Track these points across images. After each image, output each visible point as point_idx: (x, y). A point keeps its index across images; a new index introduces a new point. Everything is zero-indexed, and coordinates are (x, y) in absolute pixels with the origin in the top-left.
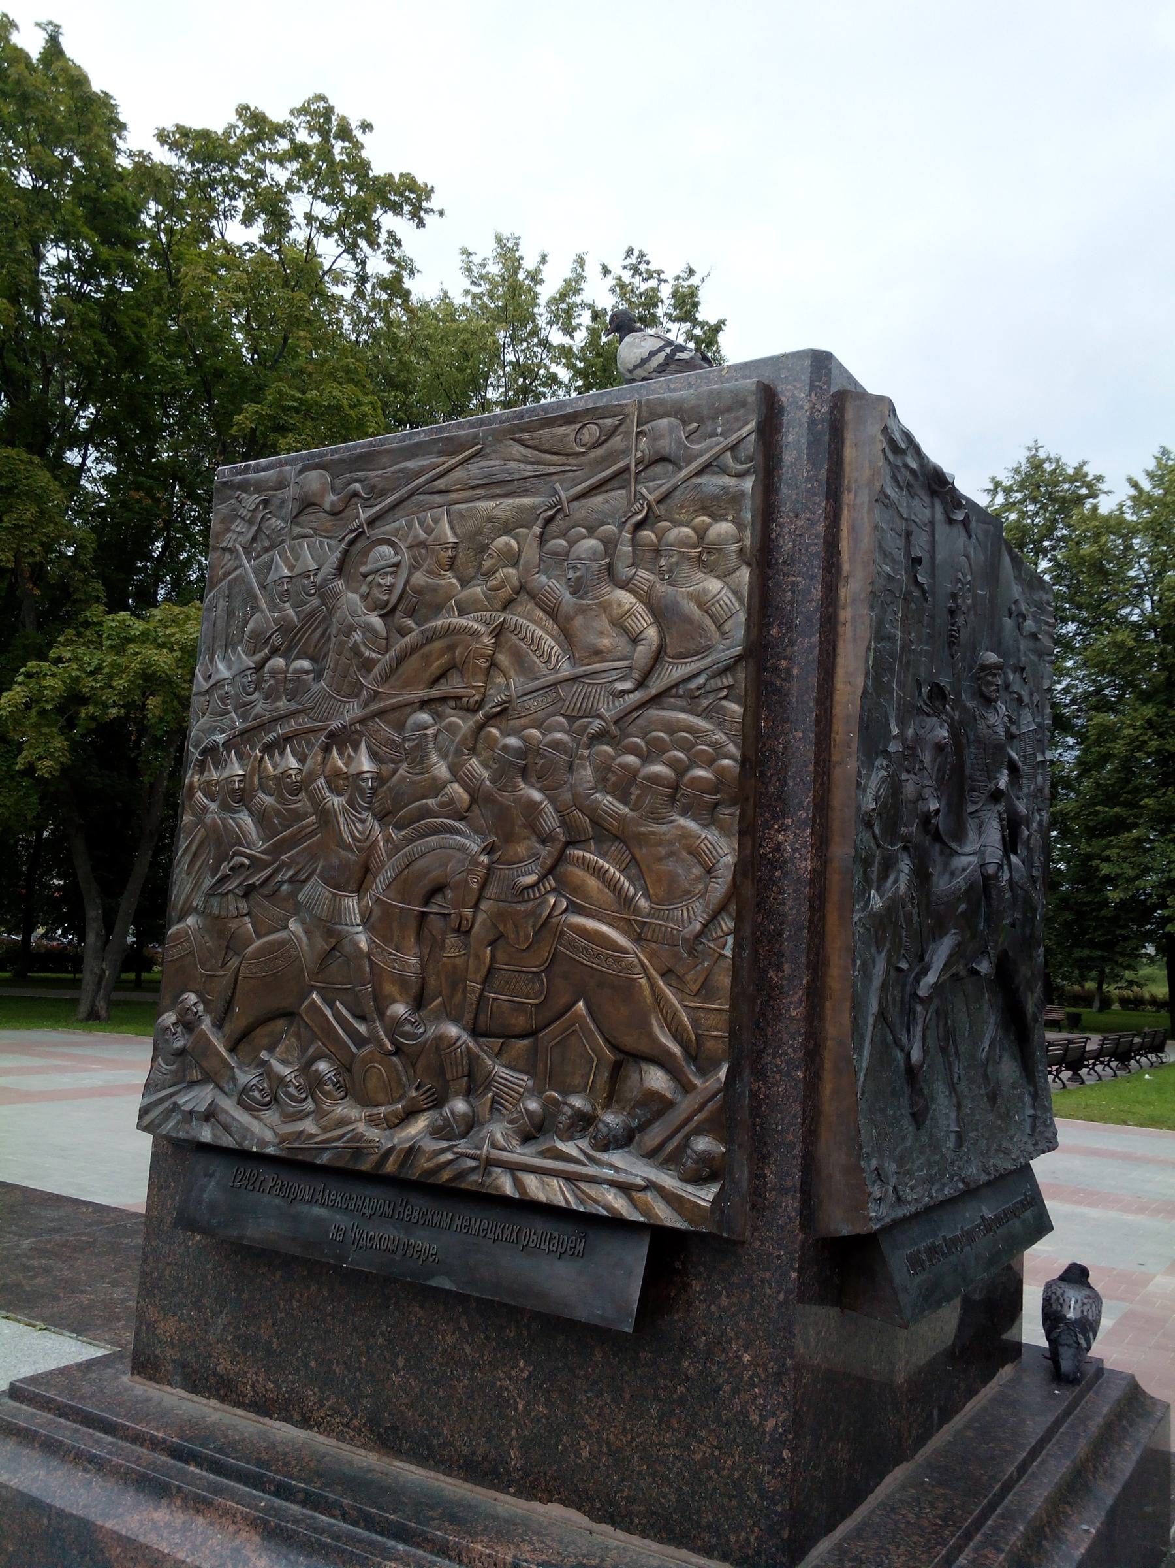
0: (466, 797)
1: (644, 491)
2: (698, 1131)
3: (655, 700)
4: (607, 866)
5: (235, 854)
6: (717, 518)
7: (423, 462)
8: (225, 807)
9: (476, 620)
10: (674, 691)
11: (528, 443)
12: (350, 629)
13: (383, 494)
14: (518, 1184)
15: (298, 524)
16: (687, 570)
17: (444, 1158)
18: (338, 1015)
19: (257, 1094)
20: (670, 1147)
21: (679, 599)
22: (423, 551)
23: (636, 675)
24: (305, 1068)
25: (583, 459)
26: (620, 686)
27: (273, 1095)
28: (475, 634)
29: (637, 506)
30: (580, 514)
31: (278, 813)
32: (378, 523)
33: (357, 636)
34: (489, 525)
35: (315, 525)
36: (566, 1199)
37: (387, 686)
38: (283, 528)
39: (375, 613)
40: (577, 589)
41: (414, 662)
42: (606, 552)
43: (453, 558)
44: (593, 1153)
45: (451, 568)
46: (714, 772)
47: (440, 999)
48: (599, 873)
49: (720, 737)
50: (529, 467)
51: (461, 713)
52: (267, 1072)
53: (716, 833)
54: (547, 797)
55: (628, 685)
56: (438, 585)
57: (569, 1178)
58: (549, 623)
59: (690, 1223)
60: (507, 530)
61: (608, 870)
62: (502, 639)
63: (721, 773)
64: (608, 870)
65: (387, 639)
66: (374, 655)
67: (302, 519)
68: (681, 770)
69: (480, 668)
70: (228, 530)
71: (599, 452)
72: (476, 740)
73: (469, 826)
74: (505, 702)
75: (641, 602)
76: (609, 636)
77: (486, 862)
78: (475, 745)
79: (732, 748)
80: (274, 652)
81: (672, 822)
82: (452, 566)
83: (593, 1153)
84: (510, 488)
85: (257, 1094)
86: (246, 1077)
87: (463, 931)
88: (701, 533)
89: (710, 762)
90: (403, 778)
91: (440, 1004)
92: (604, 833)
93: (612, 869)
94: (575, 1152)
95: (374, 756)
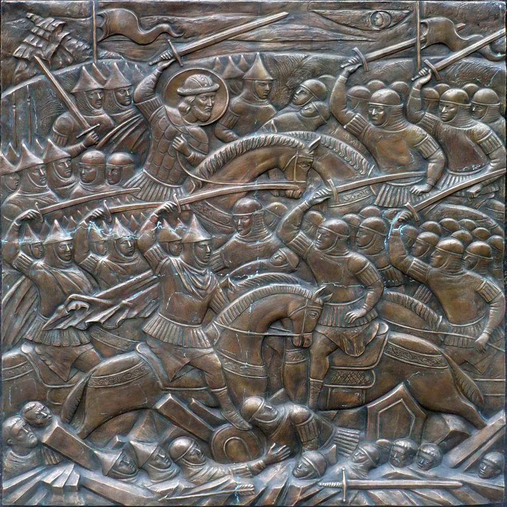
0: (296, 258)
1: (427, 61)
2: (490, 450)
3: (444, 199)
4: (416, 301)
5: (72, 300)
6: (481, 85)
7: (229, 17)
8: (53, 264)
9: (296, 136)
10: (458, 193)
11: (328, 17)
12: (173, 136)
13: (194, 35)
14: (370, 497)
15: (104, 48)
16: (463, 116)
17: (312, 491)
18: (195, 409)
19: (124, 467)
20: (472, 461)
21: (459, 134)
22: (241, 83)
23: (430, 181)
24: (165, 445)
25: (374, 35)
26: (418, 189)
27: (139, 466)
28: (297, 148)
29: (423, 71)
30: (376, 72)
31: (114, 270)
32: (190, 56)
33: (181, 141)
34: (300, 71)
35: (123, 50)
36: (412, 503)
37: (214, 178)
38: (86, 49)
39: (196, 124)
40: (381, 122)
41: (240, 162)
42: (401, 98)
43: (269, 92)
44: (422, 472)
45: (267, 97)
46: (490, 244)
47: (282, 390)
48: (411, 307)
49: (493, 222)
50: (330, 34)
51: (283, 200)
52: (129, 450)
53: (491, 278)
54: (369, 259)
55: (424, 188)
56: (257, 109)
57: (408, 489)
58: (355, 142)
59: (491, 500)
60: (314, 74)
61: (417, 304)
62: (319, 151)
63: (493, 245)
64: (417, 304)
65: (209, 144)
66: (199, 155)
67: (105, 44)
68: (466, 242)
69: (303, 171)
70: (21, 42)
71: (390, 32)
72: (302, 219)
73: (299, 277)
74: (328, 195)
75: (430, 134)
76: (407, 154)
77: (321, 301)
78: (301, 223)
79: (500, 229)
80: (90, 146)
81: (462, 274)
82: (267, 96)
83: (422, 472)
84: (315, 46)
85: (124, 467)
86: (111, 458)
87: (304, 348)
88: (471, 93)
89: (484, 237)
90: (237, 245)
91: (283, 393)
92: (410, 280)
93: (420, 304)
94: (409, 474)
95: (206, 228)
